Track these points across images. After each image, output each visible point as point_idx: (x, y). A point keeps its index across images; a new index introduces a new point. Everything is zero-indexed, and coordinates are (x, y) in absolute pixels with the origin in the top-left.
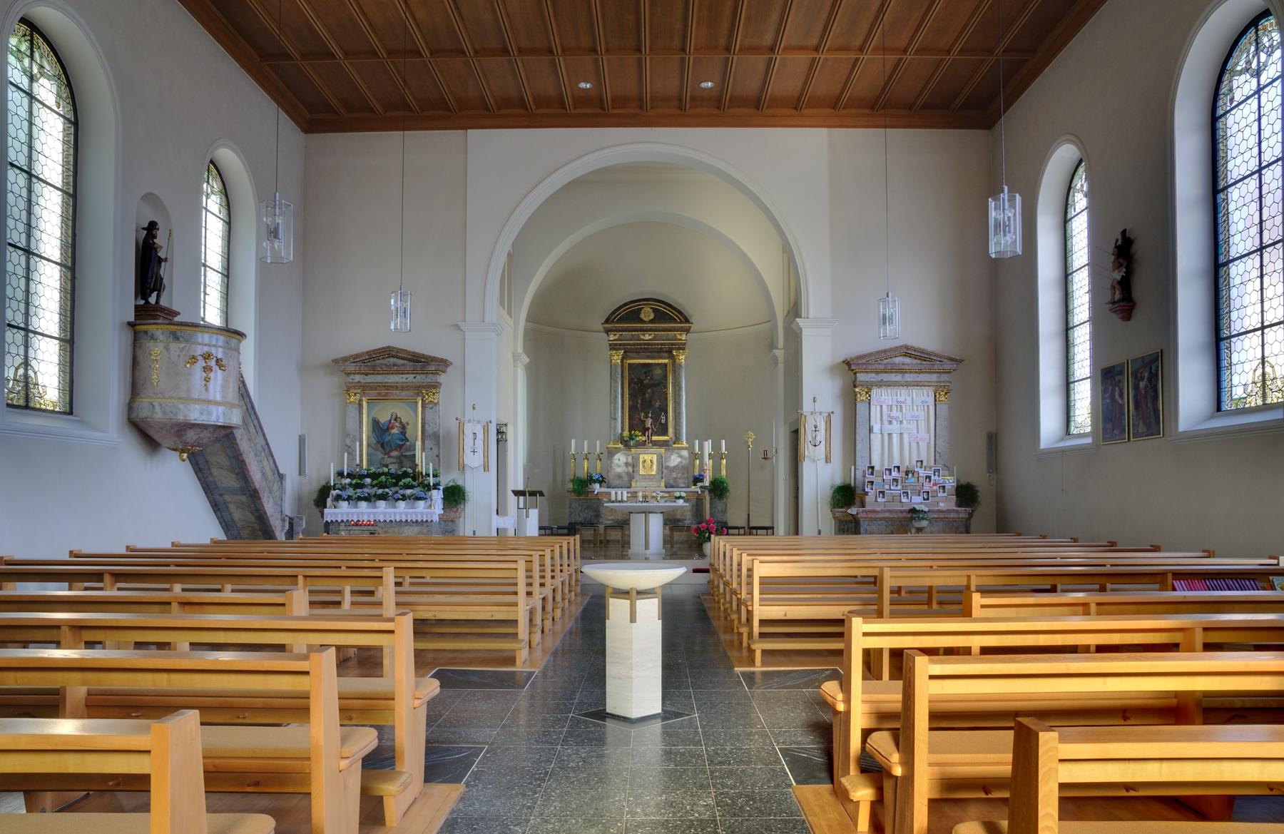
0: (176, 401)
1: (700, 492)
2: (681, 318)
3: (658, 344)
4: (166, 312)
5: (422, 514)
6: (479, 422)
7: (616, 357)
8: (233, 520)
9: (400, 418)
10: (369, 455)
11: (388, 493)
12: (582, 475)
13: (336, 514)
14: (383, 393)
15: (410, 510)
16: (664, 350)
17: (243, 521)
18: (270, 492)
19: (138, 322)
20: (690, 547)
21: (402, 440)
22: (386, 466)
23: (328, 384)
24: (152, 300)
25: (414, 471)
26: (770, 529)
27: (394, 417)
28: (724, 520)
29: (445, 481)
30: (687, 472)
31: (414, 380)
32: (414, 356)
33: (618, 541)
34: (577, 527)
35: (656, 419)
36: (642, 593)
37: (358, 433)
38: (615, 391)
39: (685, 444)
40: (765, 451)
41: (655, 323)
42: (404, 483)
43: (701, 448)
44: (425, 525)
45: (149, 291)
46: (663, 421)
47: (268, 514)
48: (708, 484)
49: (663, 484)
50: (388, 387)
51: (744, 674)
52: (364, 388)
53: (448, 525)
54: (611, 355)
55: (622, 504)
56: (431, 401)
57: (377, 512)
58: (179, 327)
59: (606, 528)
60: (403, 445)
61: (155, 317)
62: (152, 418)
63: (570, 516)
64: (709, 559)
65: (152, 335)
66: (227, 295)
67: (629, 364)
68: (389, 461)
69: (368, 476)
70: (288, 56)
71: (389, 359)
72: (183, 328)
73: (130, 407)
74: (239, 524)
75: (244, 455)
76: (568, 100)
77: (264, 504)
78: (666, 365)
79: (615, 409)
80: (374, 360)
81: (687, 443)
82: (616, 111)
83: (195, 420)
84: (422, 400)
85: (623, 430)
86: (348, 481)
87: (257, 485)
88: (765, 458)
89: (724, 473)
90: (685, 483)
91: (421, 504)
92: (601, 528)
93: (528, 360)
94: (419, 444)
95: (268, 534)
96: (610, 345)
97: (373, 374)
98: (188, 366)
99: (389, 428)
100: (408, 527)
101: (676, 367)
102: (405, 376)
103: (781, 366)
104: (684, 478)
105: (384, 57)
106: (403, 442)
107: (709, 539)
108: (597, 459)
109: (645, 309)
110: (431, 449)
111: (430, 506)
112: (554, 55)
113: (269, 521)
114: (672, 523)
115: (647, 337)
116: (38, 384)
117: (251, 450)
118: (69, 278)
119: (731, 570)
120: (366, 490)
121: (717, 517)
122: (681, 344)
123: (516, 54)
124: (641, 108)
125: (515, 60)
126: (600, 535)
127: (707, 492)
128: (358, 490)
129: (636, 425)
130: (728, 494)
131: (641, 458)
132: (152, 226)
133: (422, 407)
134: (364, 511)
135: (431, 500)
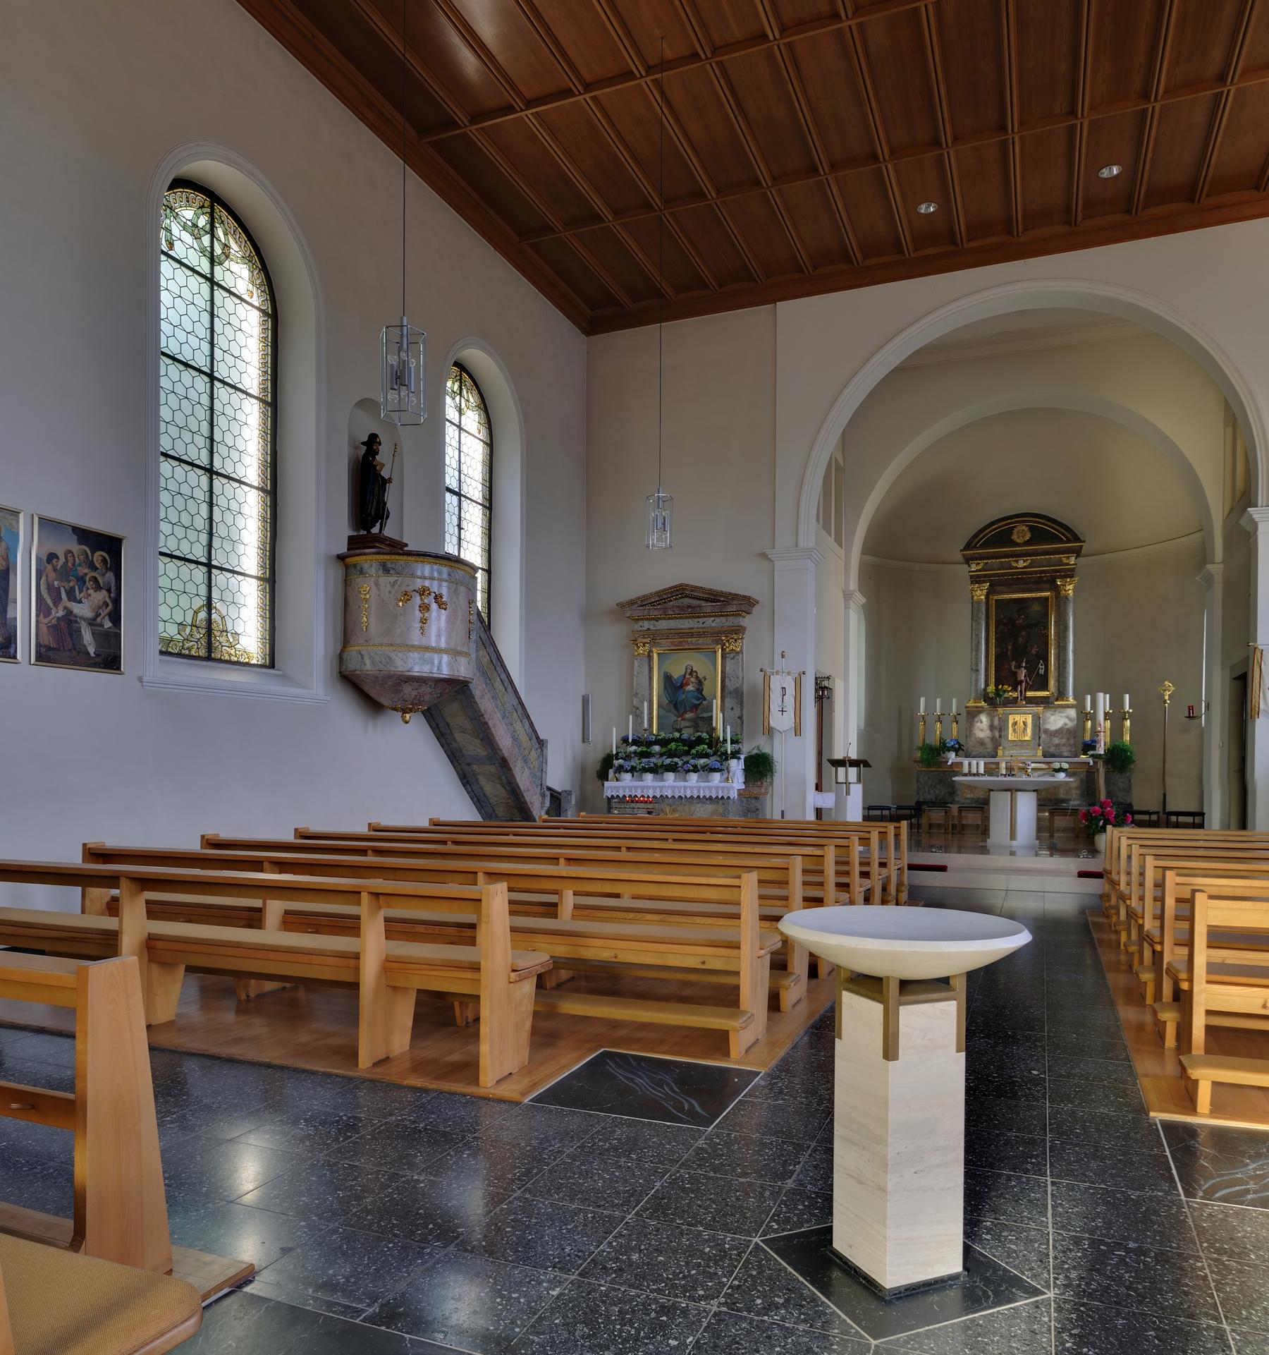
0: (387, 648)
1: (1091, 763)
2: (1069, 535)
3: (1036, 572)
4: (388, 542)
5: (717, 788)
6: (789, 674)
7: (979, 593)
8: (485, 795)
9: (696, 672)
10: (659, 717)
11: (677, 764)
12: (934, 741)
13: (617, 788)
14: (682, 642)
15: (702, 784)
16: (1045, 579)
17: (496, 796)
18: (526, 762)
19: (352, 552)
20: (1077, 837)
22: (679, 730)
23: (615, 633)
24: (375, 530)
25: (711, 736)
26: (1197, 819)
27: (689, 671)
28: (1128, 801)
29: (747, 748)
30: (1075, 737)
31: (714, 625)
32: (712, 594)
33: (978, 826)
34: (925, 807)
35: (1031, 670)
36: (912, 988)
37: (647, 691)
38: (977, 635)
39: (1071, 701)
40: (1191, 708)
42: (697, 751)
43: (1094, 705)
44: (721, 802)
46: (1042, 672)
47: (522, 788)
48: (1102, 752)
49: (1040, 753)
51: (1169, 1127)
53: (751, 800)
54: (972, 590)
55: (977, 778)
56: (732, 650)
57: (665, 786)
58: (389, 557)
59: (961, 809)
63: (918, 794)
64: (1102, 856)
65: (361, 568)
66: (490, 530)
67: (996, 600)
68: (683, 724)
69: (657, 742)
70: (549, 229)
72: (393, 557)
73: (341, 658)
74: (493, 800)
76: (906, 238)
78: (1046, 599)
79: (978, 658)
80: (665, 602)
81: (1075, 699)
82: (974, 244)
83: (408, 671)
85: (987, 684)
86: (634, 748)
87: (506, 753)
88: (1189, 717)
89: (1127, 738)
90: (1071, 751)
91: (716, 776)
92: (954, 808)
93: (864, 600)
94: (717, 703)
95: (524, 813)
96: (971, 577)
100: (700, 805)
101: (1061, 601)
103: (1218, 588)
104: (1069, 745)
105: (660, 210)
107: (1104, 829)
108: (952, 722)
109: (1019, 528)
110: (732, 709)
111: (728, 779)
112: (880, 162)
113: (523, 796)
114: (1049, 802)
115: (1021, 564)
116: (226, 631)
118: (268, 504)
119: (1142, 884)
120: (653, 760)
121: (1118, 797)
122: (1069, 570)
123: (827, 172)
124: (1010, 232)
125: (827, 179)
126: (953, 817)
127: (1100, 764)
128: (644, 760)
129: (1004, 676)
130: (1132, 767)
131: (1011, 719)
132: (373, 441)
133: (722, 657)
134: (650, 785)
135: (729, 772)
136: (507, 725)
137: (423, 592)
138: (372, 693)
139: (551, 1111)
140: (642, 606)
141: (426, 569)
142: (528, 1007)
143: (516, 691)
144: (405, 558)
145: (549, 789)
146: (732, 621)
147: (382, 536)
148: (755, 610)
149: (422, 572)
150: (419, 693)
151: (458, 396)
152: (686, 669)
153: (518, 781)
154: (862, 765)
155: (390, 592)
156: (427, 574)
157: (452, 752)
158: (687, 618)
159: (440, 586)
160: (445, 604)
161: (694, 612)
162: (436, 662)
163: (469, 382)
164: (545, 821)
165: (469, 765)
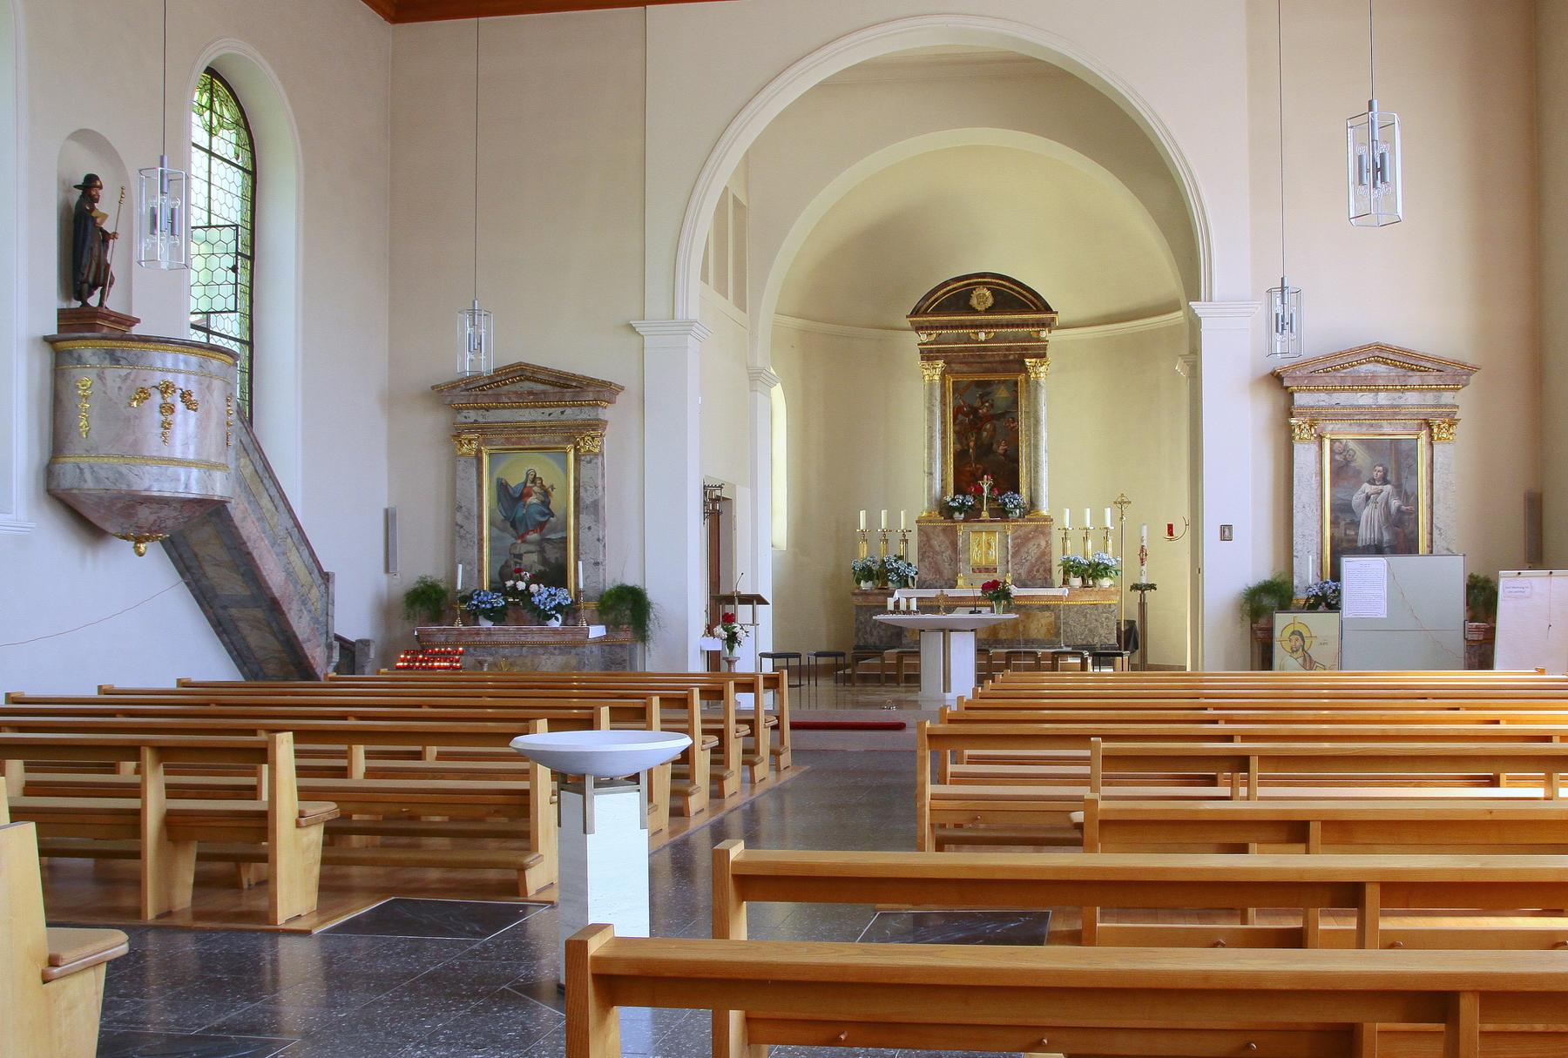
3: (999, 349)
4: (113, 318)
8: (248, 648)
10: (491, 539)
14: (518, 439)
18: (304, 603)
21: (544, 515)
23: (430, 424)
24: (93, 301)
27: (531, 477)
32: (560, 378)
41: (994, 314)
45: (86, 285)
47: (300, 638)
50: (519, 428)
52: (483, 430)
60: (546, 522)
61: (92, 328)
62: (79, 490)
63: (857, 635)
65: (79, 356)
68: (522, 548)
71: (521, 384)
72: (124, 344)
75: (248, 544)
77: (291, 622)
80: (498, 386)
84: (577, 450)
95: (304, 669)
97: (497, 408)
98: (135, 404)
99: (524, 495)
102: (547, 411)
106: (547, 518)
110: (589, 528)
113: (302, 649)
115: (982, 336)
117: (263, 535)
132: (90, 183)
133: (575, 460)
136: (277, 555)
137: (166, 389)
138: (93, 517)
139: (339, 938)
140: (468, 390)
141: (169, 359)
142: (317, 854)
143: (290, 511)
144: (141, 345)
145: (338, 638)
146: (585, 414)
147: (105, 311)
148: (620, 398)
149: (164, 362)
150: (159, 517)
151: (208, 112)
152: (527, 475)
153: (295, 629)
154: (755, 602)
155: (120, 388)
156: (169, 365)
157: (202, 593)
158: (527, 407)
159: (187, 381)
160: (196, 404)
161: (538, 400)
162: (183, 478)
163: (223, 91)
164: (332, 679)
165: (225, 608)
